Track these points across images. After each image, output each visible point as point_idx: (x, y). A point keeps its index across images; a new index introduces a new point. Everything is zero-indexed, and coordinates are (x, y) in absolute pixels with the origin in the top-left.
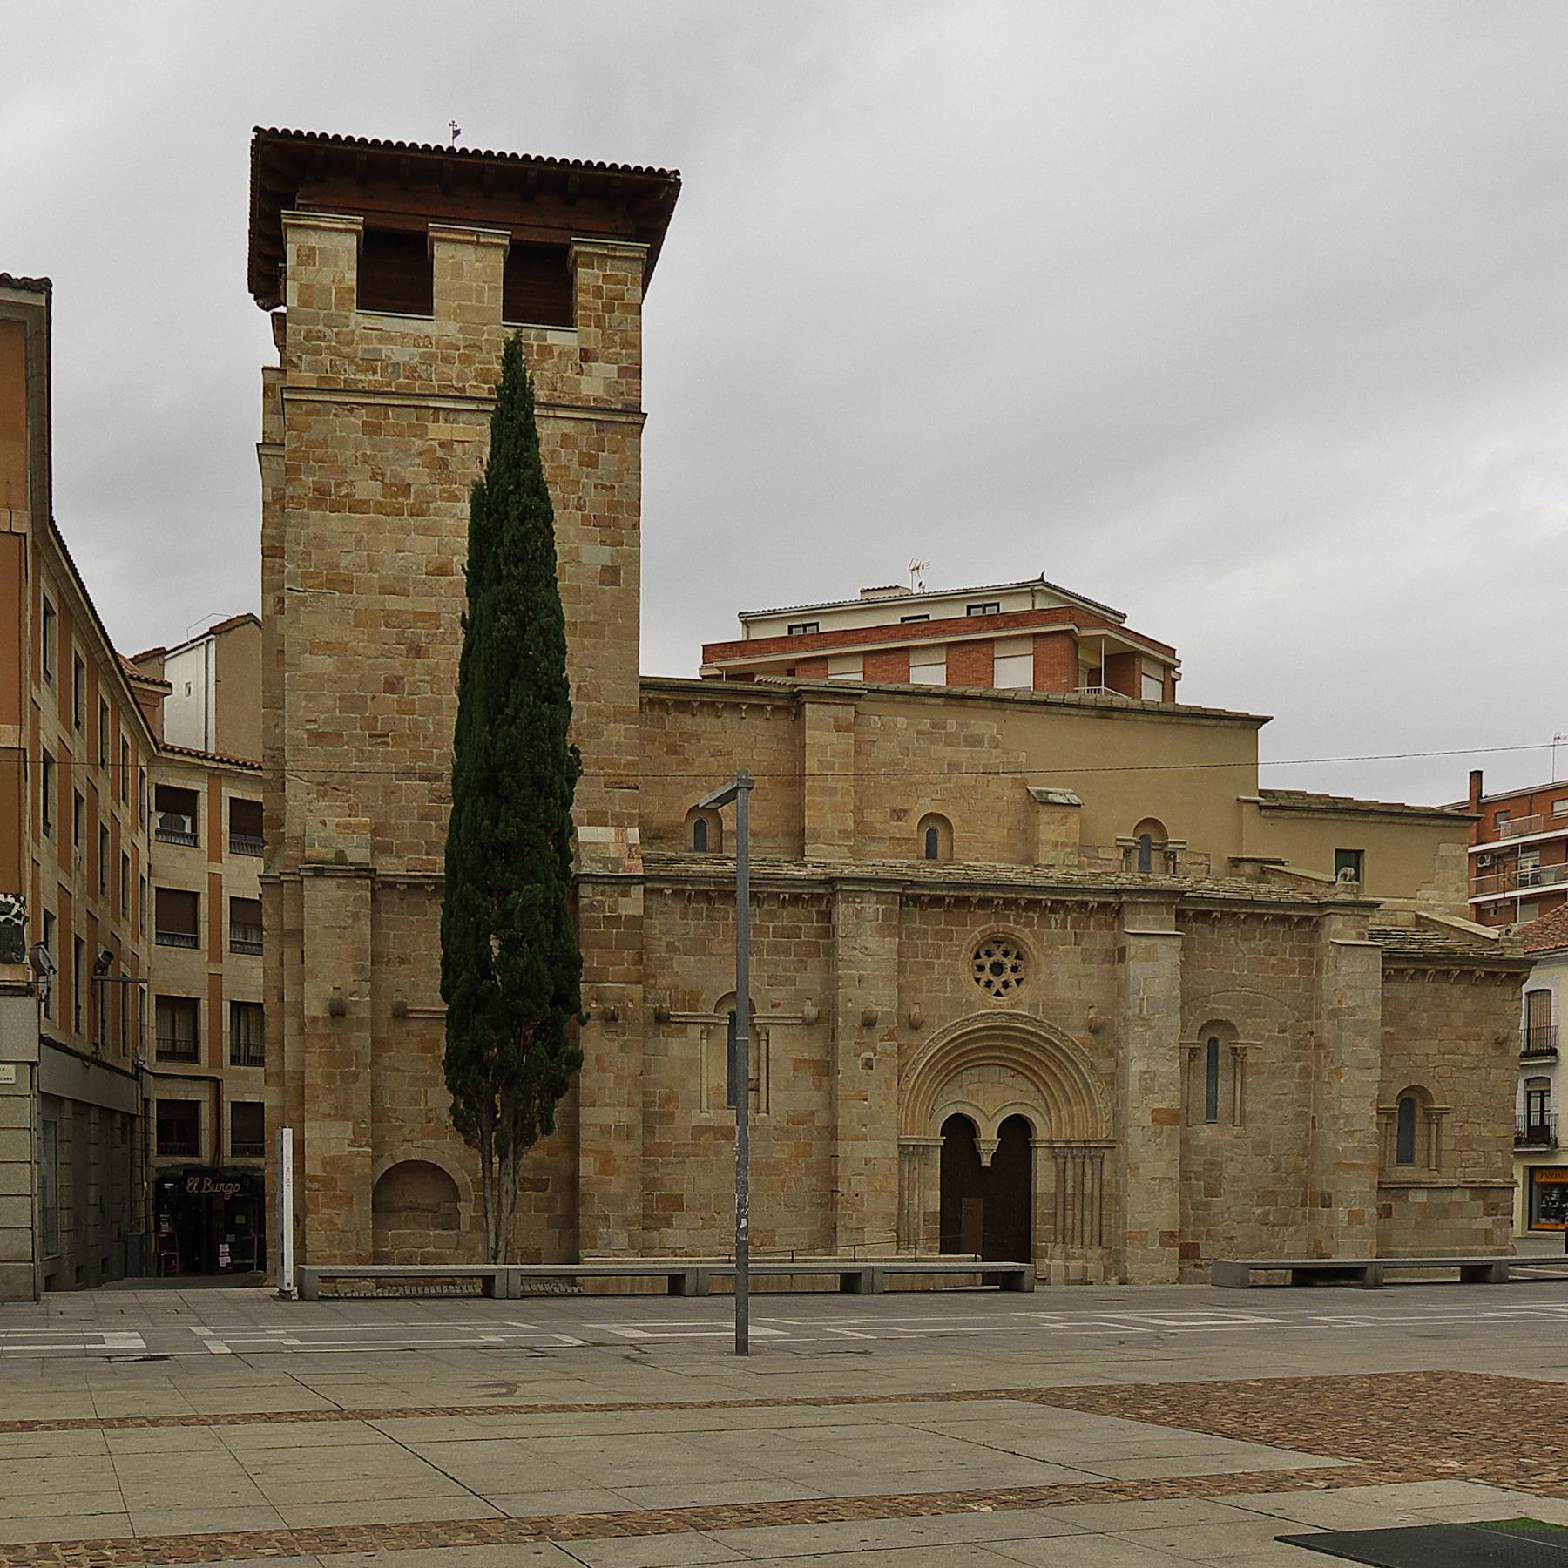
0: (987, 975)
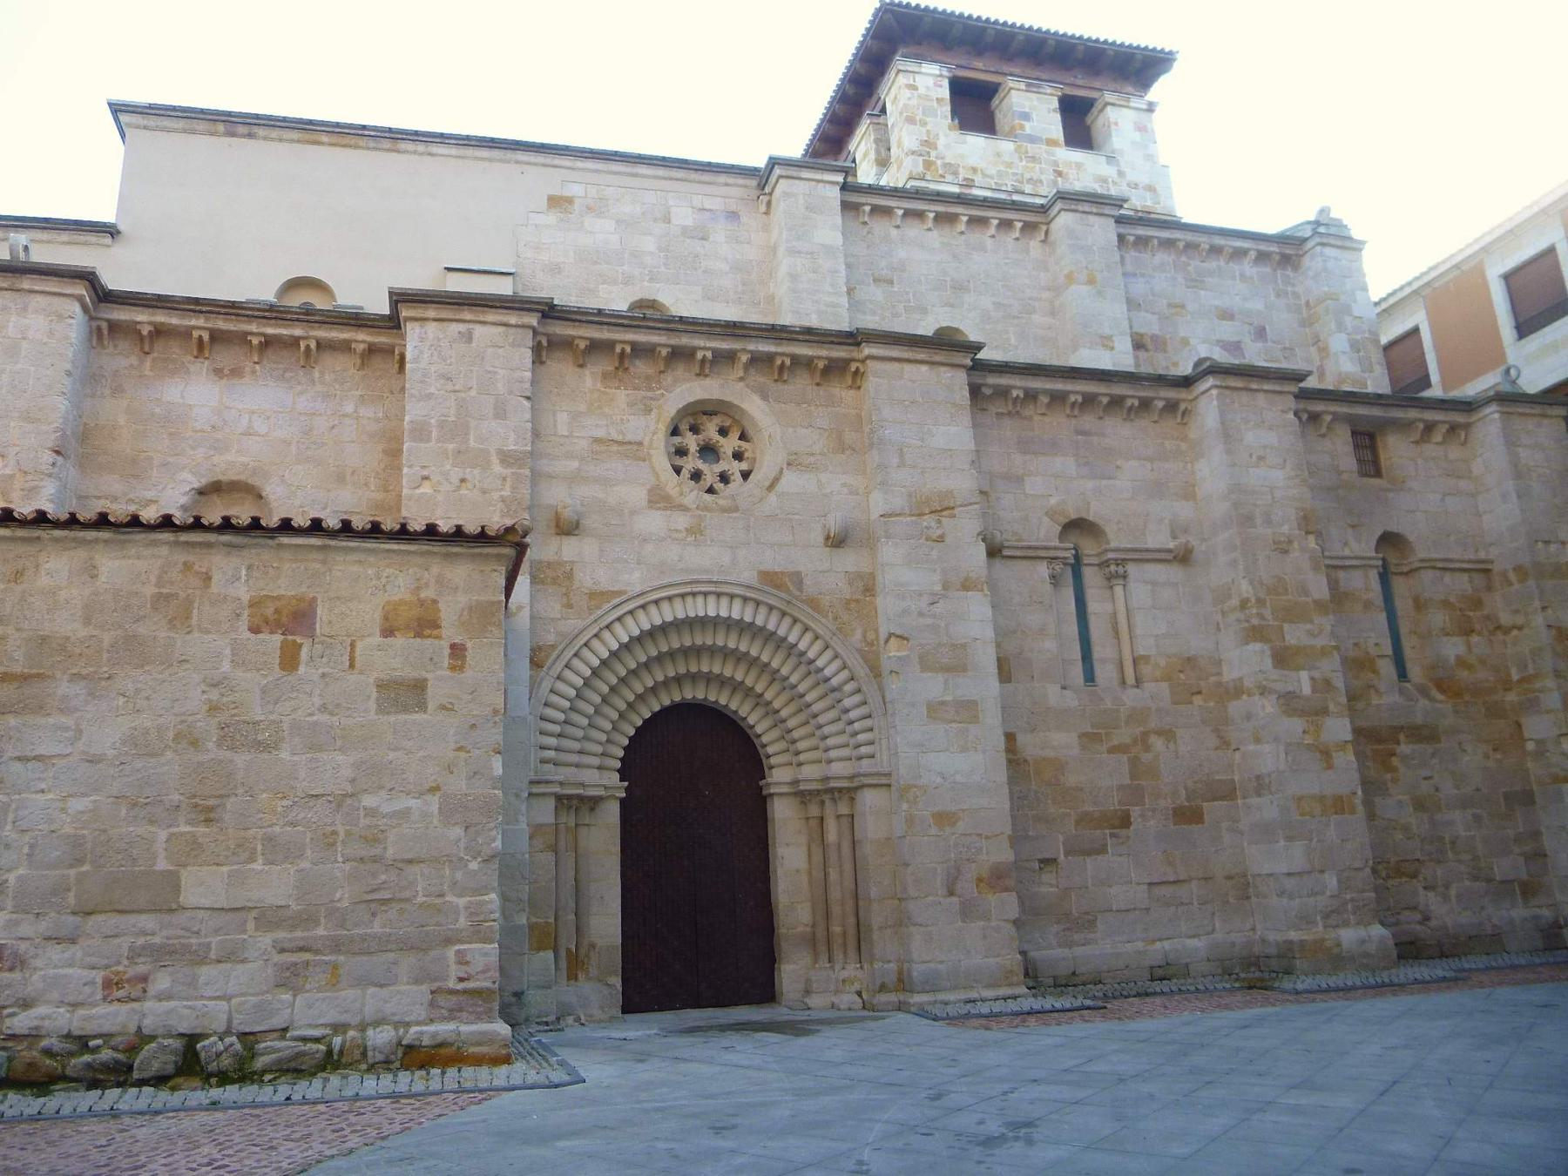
0: (691, 463)
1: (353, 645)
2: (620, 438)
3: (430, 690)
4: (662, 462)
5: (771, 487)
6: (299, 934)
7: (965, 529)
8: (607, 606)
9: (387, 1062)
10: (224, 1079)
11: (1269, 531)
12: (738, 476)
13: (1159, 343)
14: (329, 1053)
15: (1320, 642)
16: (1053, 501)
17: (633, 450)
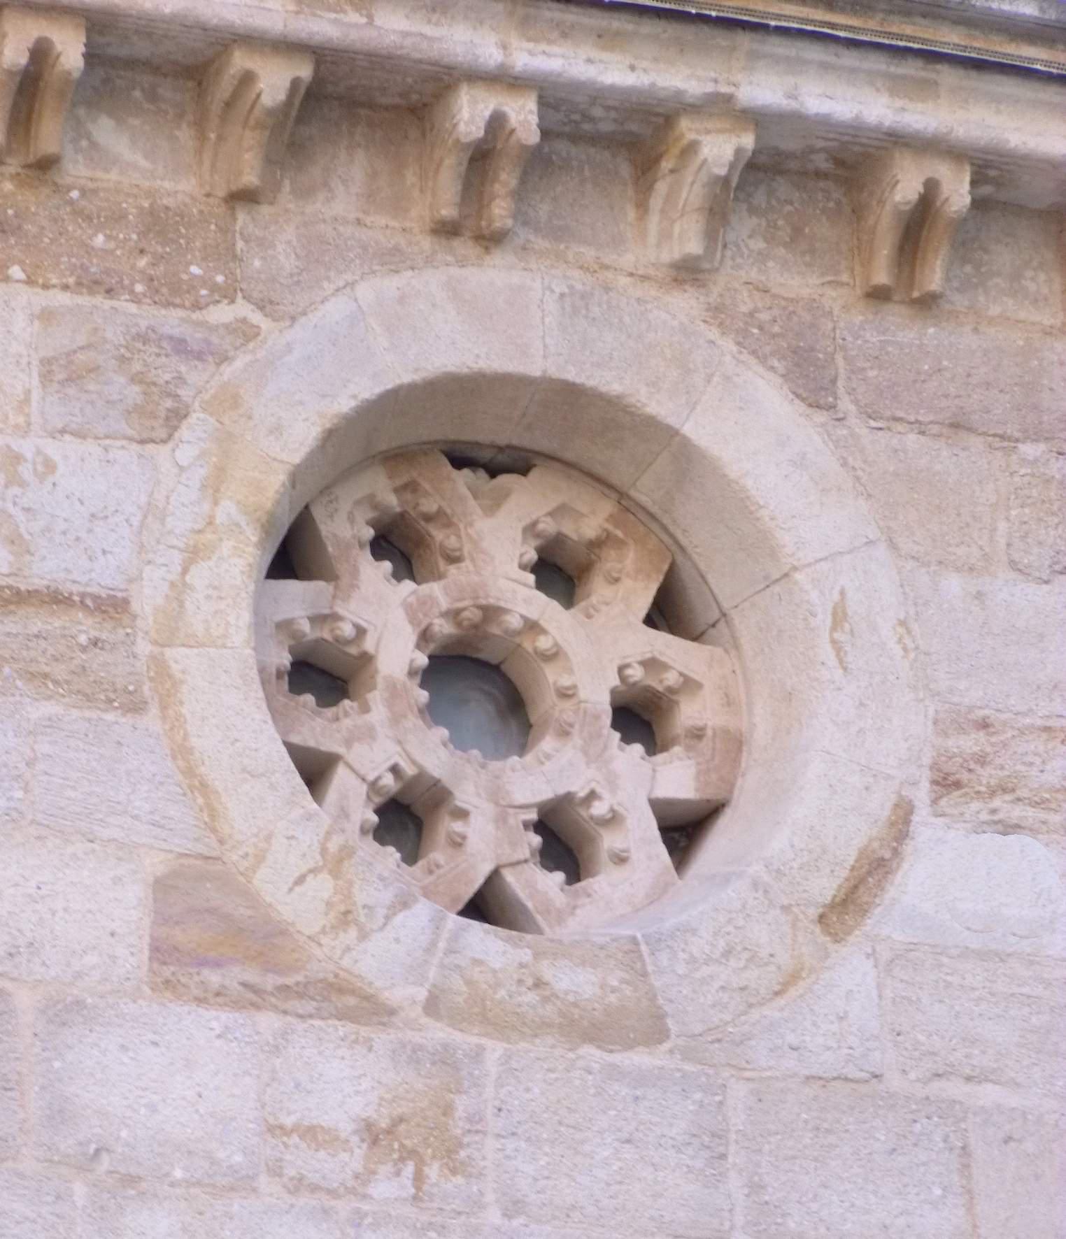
0: (387, 737)
5: (846, 908)
12: (642, 837)
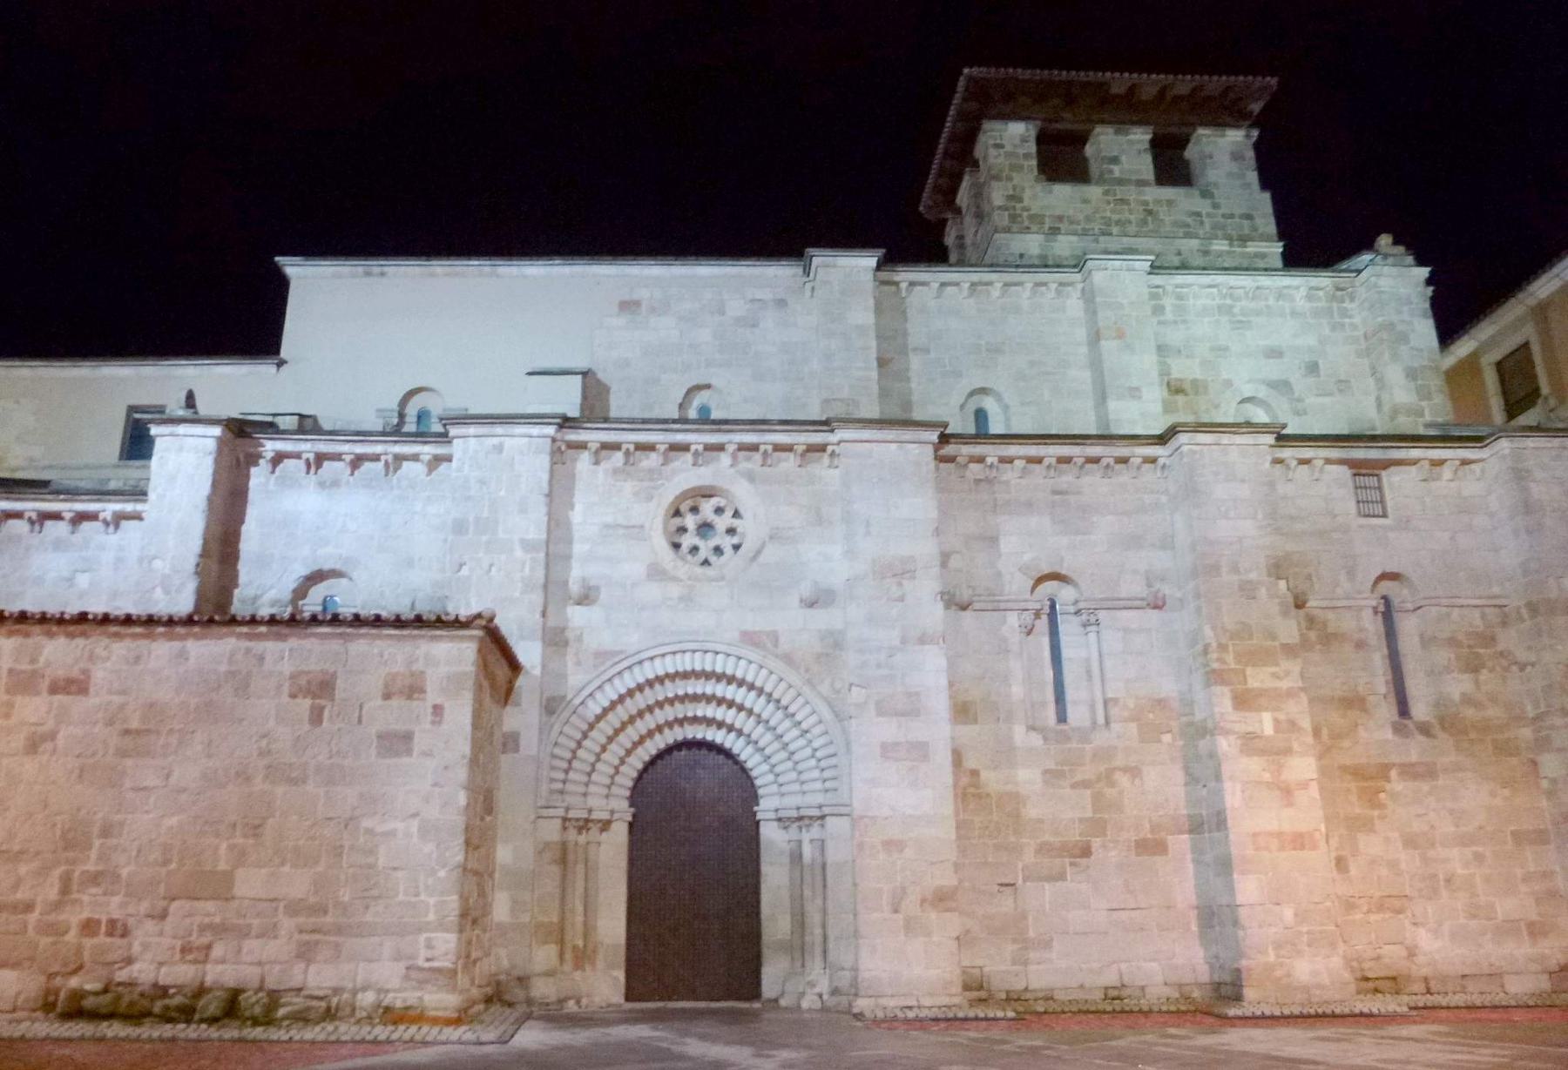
1: (361, 707)
2: (625, 523)
3: (416, 740)
4: (661, 544)
6: (313, 920)
7: (926, 588)
8: (609, 663)
9: (370, 1017)
10: (256, 1022)
11: (1236, 578)
13: (1198, 387)
14: (328, 1009)
15: (1285, 684)
16: (1027, 557)
17: (635, 531)
